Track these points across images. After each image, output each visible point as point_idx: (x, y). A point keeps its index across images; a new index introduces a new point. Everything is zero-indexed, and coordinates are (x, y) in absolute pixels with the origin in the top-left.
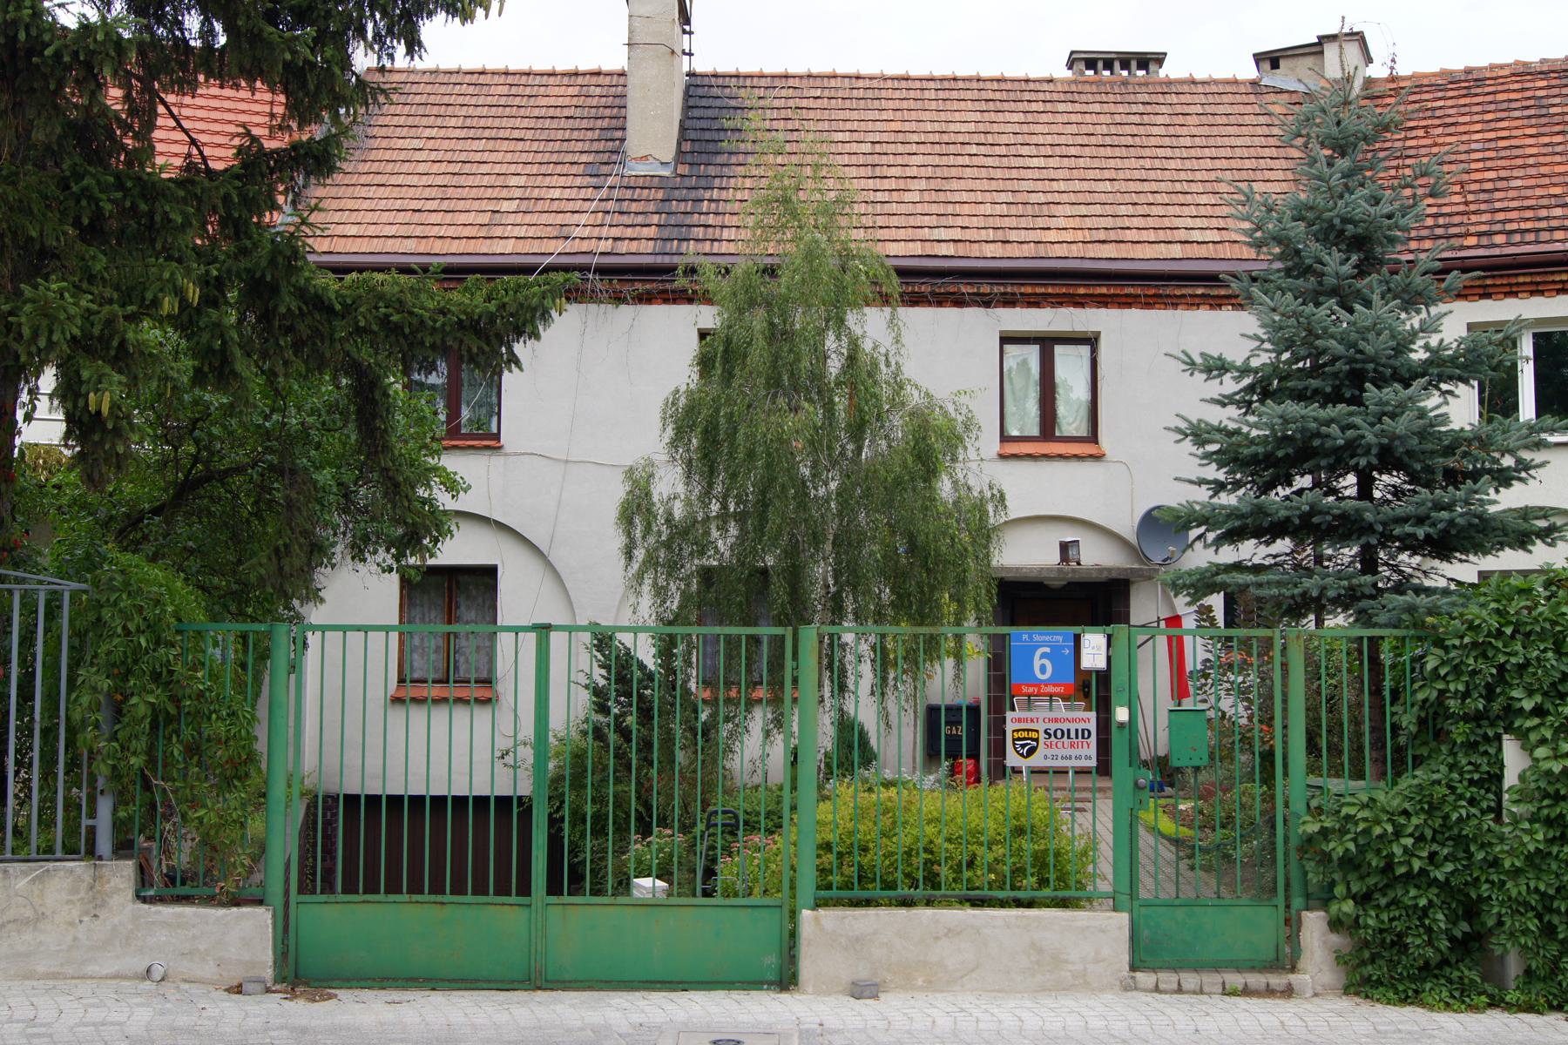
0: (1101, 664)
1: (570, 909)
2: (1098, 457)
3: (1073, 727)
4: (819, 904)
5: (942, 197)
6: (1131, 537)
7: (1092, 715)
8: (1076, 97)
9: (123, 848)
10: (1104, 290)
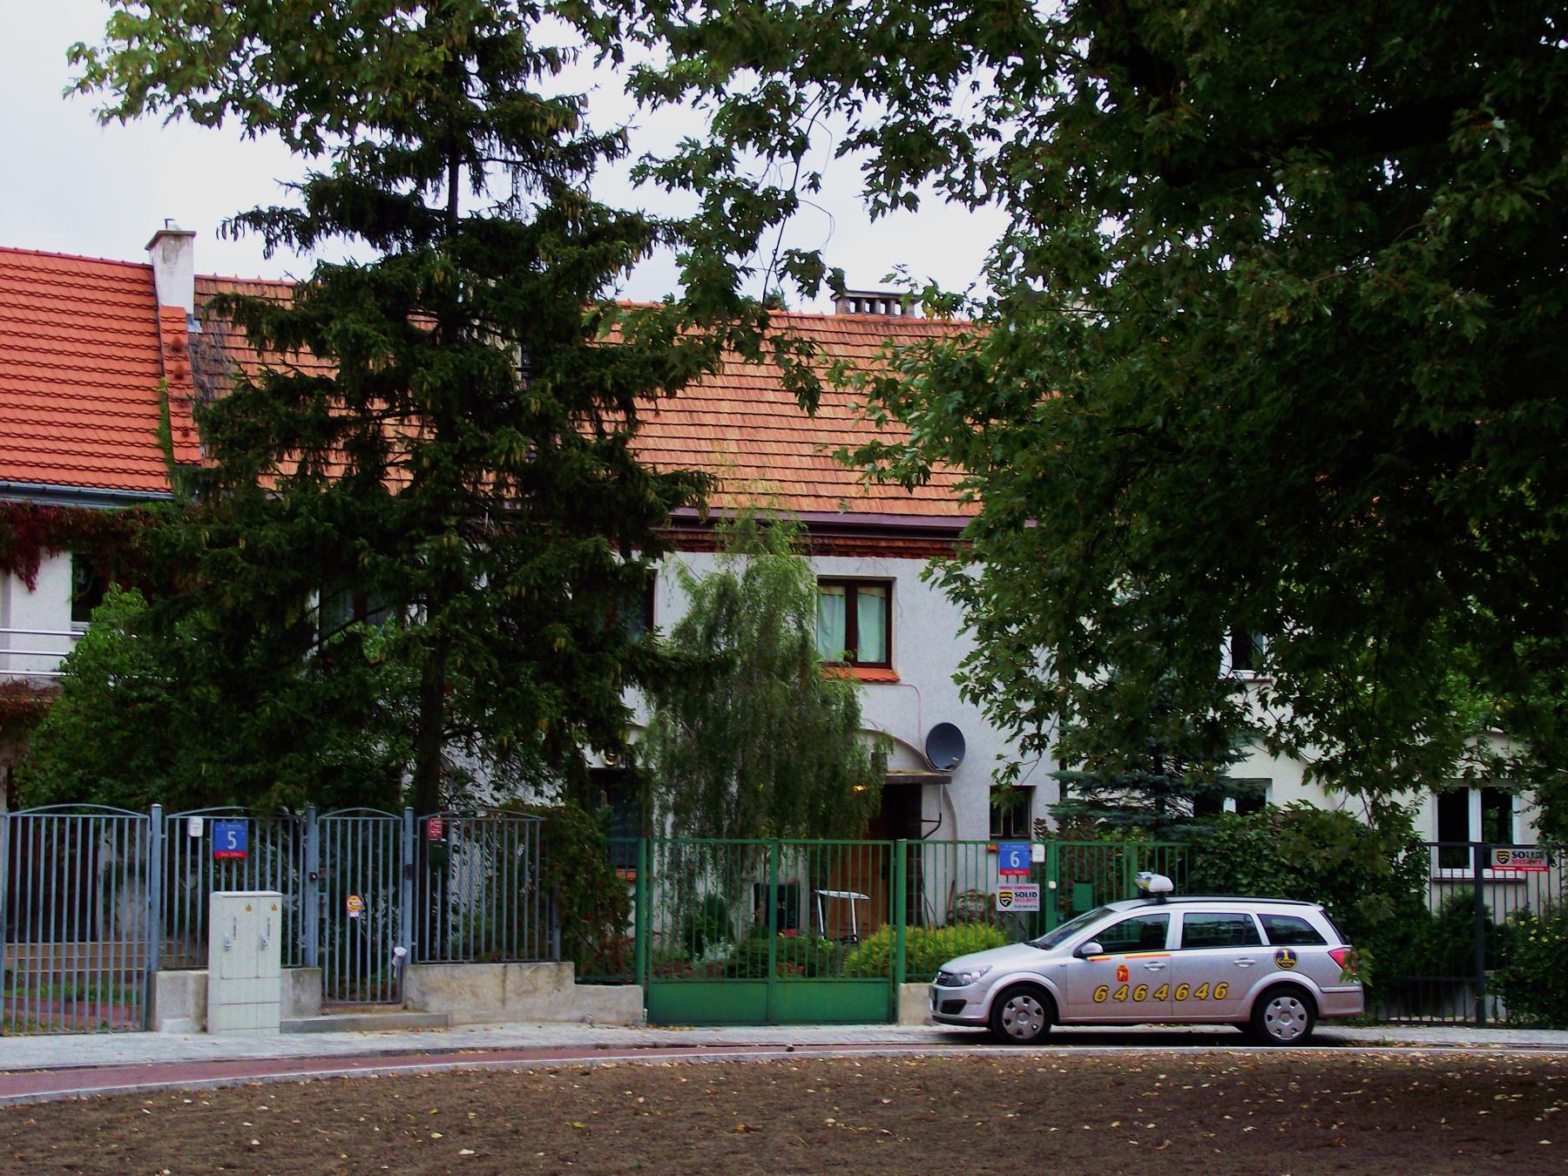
0: (1042, 859)
1: (788, 985)
2: (894, 681)
3: (1028, 891)
4: (908, 980)
5: (754, 447)
6: (921, 748)
7: (1037, 885)
8: (847, 338)
9: (565, 957)
10: (901, 544)
